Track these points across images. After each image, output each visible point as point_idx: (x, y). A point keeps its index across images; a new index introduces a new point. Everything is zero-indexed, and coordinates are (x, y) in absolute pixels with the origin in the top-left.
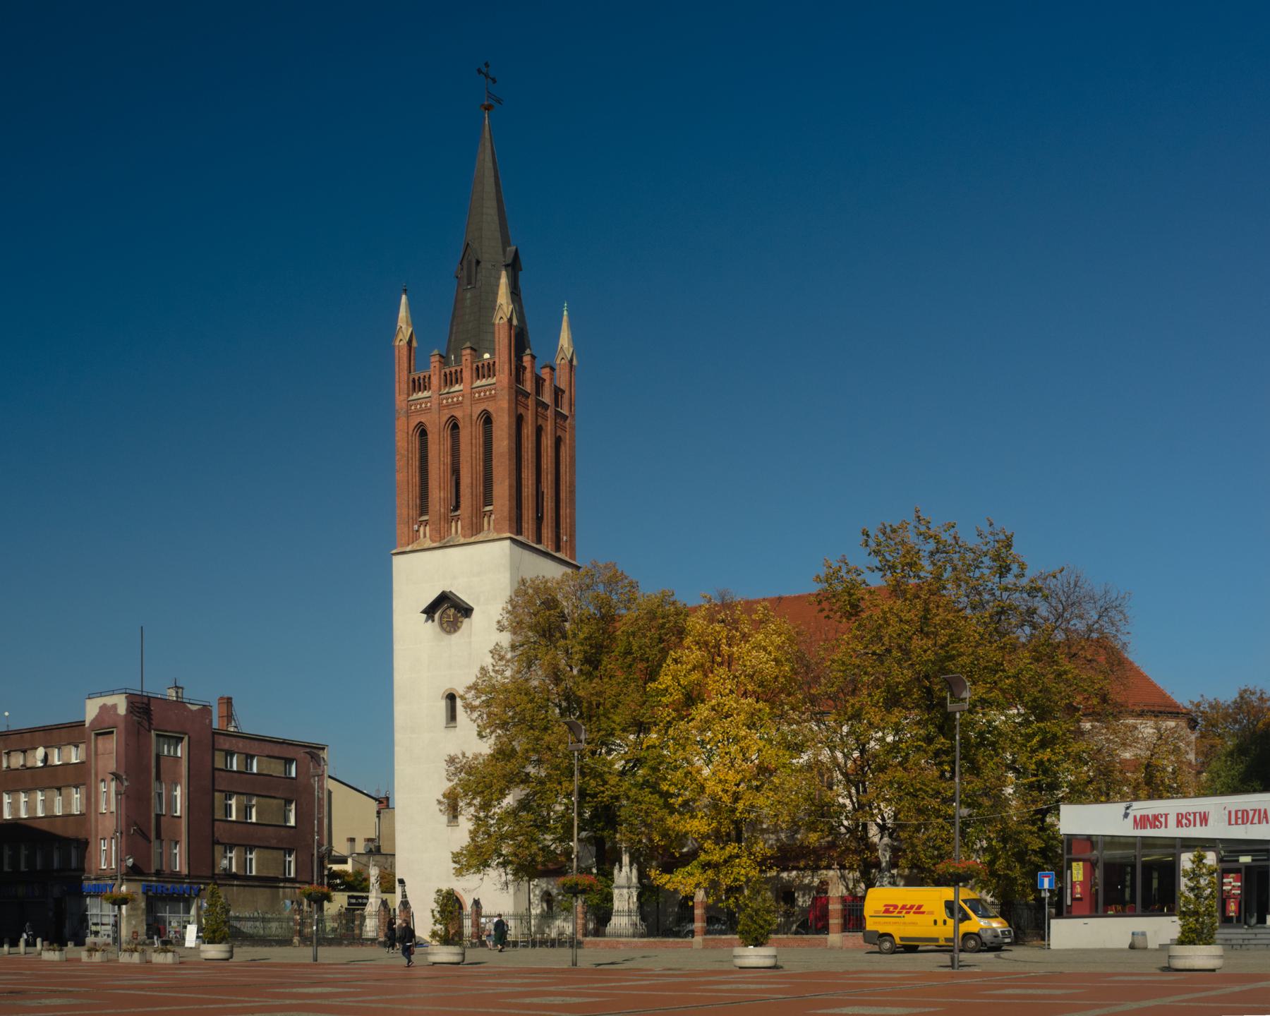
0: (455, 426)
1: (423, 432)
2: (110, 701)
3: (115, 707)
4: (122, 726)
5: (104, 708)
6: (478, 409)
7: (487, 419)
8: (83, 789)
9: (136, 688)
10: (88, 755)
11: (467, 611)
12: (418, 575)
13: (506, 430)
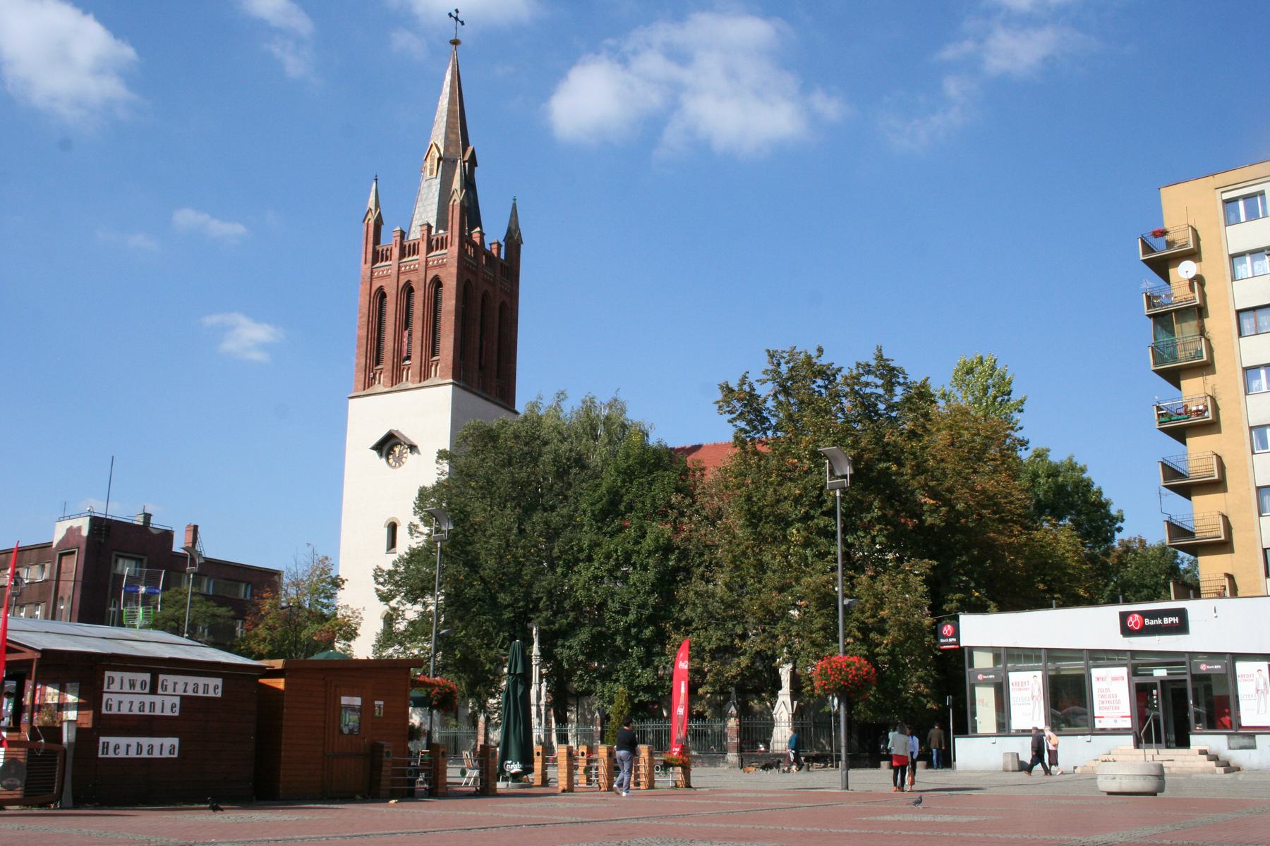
0: (408, 289)
1: (381, 295)
2: (75, 523)
3: (79, 529)
4: (83, 547)
5: (70, 530)
6: (403, 280)
7: (437, 283)
8: (43, 605)
9: (100, 511)
10: (51, 574)
11: (413, 448)
12: (372, 414)
13: (454, 292)
